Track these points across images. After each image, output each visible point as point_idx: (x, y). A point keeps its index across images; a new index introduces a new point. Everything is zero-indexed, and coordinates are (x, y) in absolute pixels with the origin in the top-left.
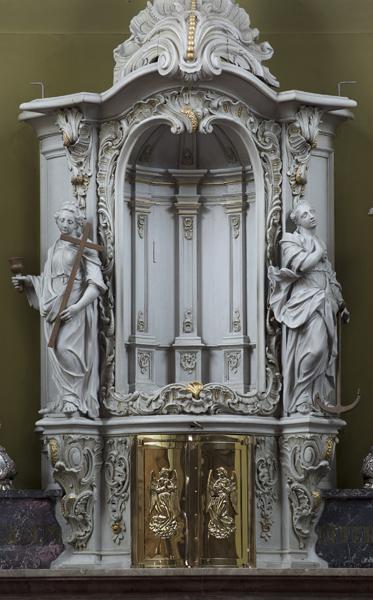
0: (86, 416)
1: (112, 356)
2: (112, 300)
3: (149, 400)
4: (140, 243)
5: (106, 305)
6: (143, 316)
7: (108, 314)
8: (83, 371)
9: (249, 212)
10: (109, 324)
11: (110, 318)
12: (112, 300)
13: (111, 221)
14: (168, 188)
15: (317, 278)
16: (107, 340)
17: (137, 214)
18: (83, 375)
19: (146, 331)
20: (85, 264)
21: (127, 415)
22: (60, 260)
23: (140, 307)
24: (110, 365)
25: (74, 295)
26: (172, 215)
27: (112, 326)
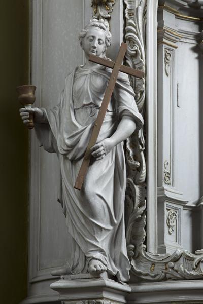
0: (115, 278)
1: (144, 208)
2: (143, 142)
3: (196, 261)
4: (166, 80)
5: (134, 146)
6: (168, 167)
7: (137, 157)
8: (112, 223)
9: (75, 83)
10: (139, 169)
11: (141, 162)
12: (143, 142)
13: (143, 48)
14: (191, 24)
15: (110, 232)
16: (137, 188)
17: (164, 45)
18: (111, 228)
19: (173, 185)
20: (118, 92)
21: (165, 279)
22: (87, 87)
23: (166, 157)
24: (140, 219)
25: (106, 128)
26: (196, 55)
27: (144, 172)
